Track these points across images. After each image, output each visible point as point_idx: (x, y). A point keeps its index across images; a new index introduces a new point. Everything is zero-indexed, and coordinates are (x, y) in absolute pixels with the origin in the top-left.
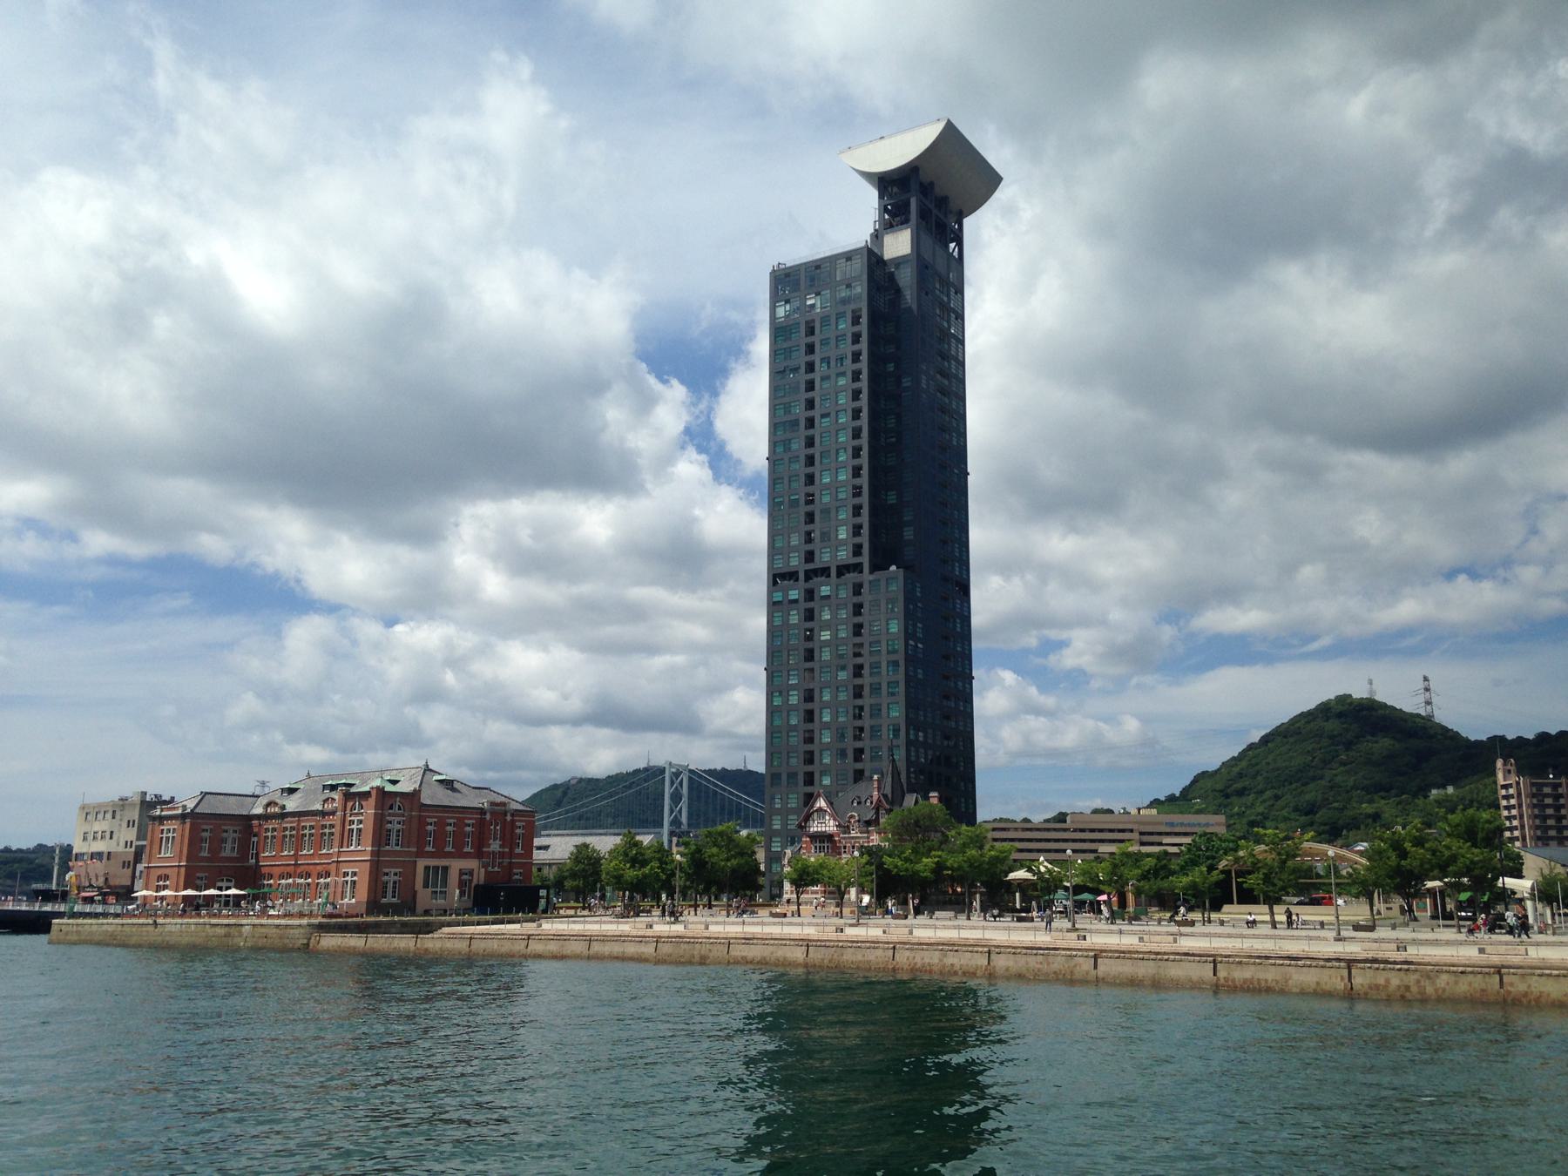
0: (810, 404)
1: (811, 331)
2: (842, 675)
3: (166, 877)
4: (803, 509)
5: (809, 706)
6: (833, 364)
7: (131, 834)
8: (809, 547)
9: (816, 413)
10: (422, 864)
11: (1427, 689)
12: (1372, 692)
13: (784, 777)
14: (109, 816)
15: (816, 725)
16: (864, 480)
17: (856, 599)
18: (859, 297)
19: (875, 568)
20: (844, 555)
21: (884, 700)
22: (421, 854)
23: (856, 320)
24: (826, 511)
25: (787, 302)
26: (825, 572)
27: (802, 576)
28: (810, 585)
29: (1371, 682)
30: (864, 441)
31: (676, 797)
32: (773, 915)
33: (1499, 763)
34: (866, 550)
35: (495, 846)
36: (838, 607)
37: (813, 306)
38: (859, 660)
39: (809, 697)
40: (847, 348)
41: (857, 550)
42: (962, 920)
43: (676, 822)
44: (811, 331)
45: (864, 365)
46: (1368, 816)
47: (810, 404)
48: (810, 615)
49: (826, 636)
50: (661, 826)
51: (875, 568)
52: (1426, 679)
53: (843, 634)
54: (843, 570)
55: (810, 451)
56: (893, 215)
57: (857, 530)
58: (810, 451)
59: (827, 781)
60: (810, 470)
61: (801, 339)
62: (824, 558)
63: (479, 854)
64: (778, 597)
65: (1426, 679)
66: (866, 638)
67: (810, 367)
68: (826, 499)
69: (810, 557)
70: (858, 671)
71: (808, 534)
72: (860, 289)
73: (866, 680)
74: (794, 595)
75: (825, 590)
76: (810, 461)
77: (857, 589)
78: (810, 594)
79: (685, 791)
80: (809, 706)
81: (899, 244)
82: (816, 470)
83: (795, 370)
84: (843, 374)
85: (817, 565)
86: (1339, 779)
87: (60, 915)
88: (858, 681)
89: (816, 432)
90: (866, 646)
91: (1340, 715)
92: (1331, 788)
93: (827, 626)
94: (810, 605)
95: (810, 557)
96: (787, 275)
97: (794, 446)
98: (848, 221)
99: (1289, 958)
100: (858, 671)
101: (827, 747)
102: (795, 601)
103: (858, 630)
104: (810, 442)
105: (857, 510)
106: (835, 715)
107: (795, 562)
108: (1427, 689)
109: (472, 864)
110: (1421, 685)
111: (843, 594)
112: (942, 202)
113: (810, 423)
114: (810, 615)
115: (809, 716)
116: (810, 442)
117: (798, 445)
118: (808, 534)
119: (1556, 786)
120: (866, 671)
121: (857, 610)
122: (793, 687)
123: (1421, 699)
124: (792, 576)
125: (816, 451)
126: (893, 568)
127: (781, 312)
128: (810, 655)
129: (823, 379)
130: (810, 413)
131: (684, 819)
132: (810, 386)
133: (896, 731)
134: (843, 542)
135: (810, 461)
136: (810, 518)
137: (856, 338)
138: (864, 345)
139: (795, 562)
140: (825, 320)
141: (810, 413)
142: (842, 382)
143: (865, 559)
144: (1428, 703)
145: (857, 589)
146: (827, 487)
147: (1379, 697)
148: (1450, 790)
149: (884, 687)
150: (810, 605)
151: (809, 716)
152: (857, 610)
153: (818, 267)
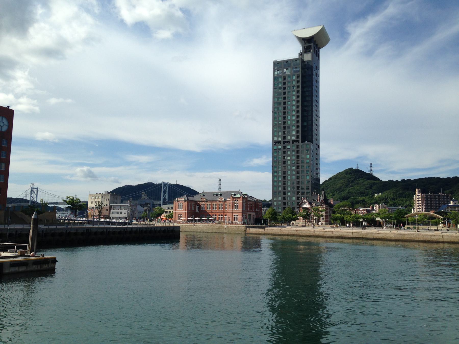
0: (285, 98)
1: (285, 79)
2: (294, 168)
3: (181, 215)
4: (282, 126)
5: (284, 175)
6: (291, 88)
7: (108, 202)
8: (284, 135)
9: (286, 101)
10: (248, 213)
11: (371, 167)
12: (358, 167)
13: (277, 193)
14: (100, 197)
15: (286, 180)
16: (300, 119)
17: (297, 149)
18: (299, 71)
19: (302, 142)
20: (294, 138)
21: (305, 175)
22: (248, 211)
23: (298, 77)
24: (289, 127)
25: (278, 70)
26: (289, 142)
27: (282, 143)
28: (284, 145)
29: (357, 165)
30: (300, 109)
31: (165, 192)
32: (331, 227)
33: (417, 190)
34: (300, 137)
35: (257, 210)
36: (293, 151)
37: (285, 72)
38: (298, 165)
39: (284, 173)
40: (295, 83)
41: (298, 137)
42: (358, 228)
43: (165, 199)
44: (285, 79)
45: (300, 89)
46: (361, 201)
47: (285, 98)
48: (284, 153)
49: (289, 158)
50: (161, 200)
51: (302, 142)
52: (371, 164)
53: (294, 158)
54: (293, 142)
55: (284, 111)
56: (306, 50)
57: (298, 132)
58: (284, 111)
59: (289, 194)
60: (284, 116)
61: (281, 80)
62: (289, 138)
63: (255, 212)
64: (275, 147)
65: (371, 164)
66: (300, 159)
67: (285, 88)
68: (289, 123)
69: (284, 138)
70: (298, 167)
71: (284, 132)
72: (300, 69)
73: (300, 169)
74: (280, 147)
75: (289, 147)
76: (284, 113)
77: (298, 147)
78: (284, 147)
79: (167, 190)
80: (284, 175)
81: (308, 57)
82: (286, 115)
83: (280, 88)
84: (294, 91)
85: (286, 140)
86: (351, 191)
87: (240, 224)
88: (298, 170)
89: (286, 106)
90: (300, 161)
91: (350, 173)
92: (349, 193)
93: (289, 156)
94: (284, 150)
95: (284, 138)
96: (278, 63)
97: (280, 109)
98: (293, 51)
99: (363, 238)
100: (298, 167)
101: (289, 186)
102: (280, 149)
103: (298, 157)
104: (284, 108)
105: (298, 127)
106: (291, 178)
107: (280, 139)
108: (371, 167)
109: (254, 214)
110: (300, 154)
111: (294, 148)
112: (317, 45)
113: (285, 103)
114: (284, 153)
115: (284, 178)
116: (284, 108)
117: (281, 109)
118: (284, 132)
119: (431, 196)
120: (300, 167)
121: (298, 152)
122: (280, 171)
123: (370, 169)
124: (279, 142)
125: (286, 111)
126: (306, 142)
127: (276, 73)
128: (284, 163)
129: (288, 92)
130: (284, 101)
131: (167, 198)
132: (285, 93)
133: (308, 182)
134: (294, 135)
135: (284, 113)
136: (284, 128)
137: (298, 82)
138: (300, 84)
139: (280, 139)
140: (289, 76)
141: (284, 101)
142: (294, 93)
143: (300, 139)
144: (371, 170)
145: (298, 147)
146: (289, 120)
147: (360, 169)
148: (380, 194)
149: (305, 171)
150: (284, 150)
151: (284, 178)
152: (298, 152)
153: (287, 62)
